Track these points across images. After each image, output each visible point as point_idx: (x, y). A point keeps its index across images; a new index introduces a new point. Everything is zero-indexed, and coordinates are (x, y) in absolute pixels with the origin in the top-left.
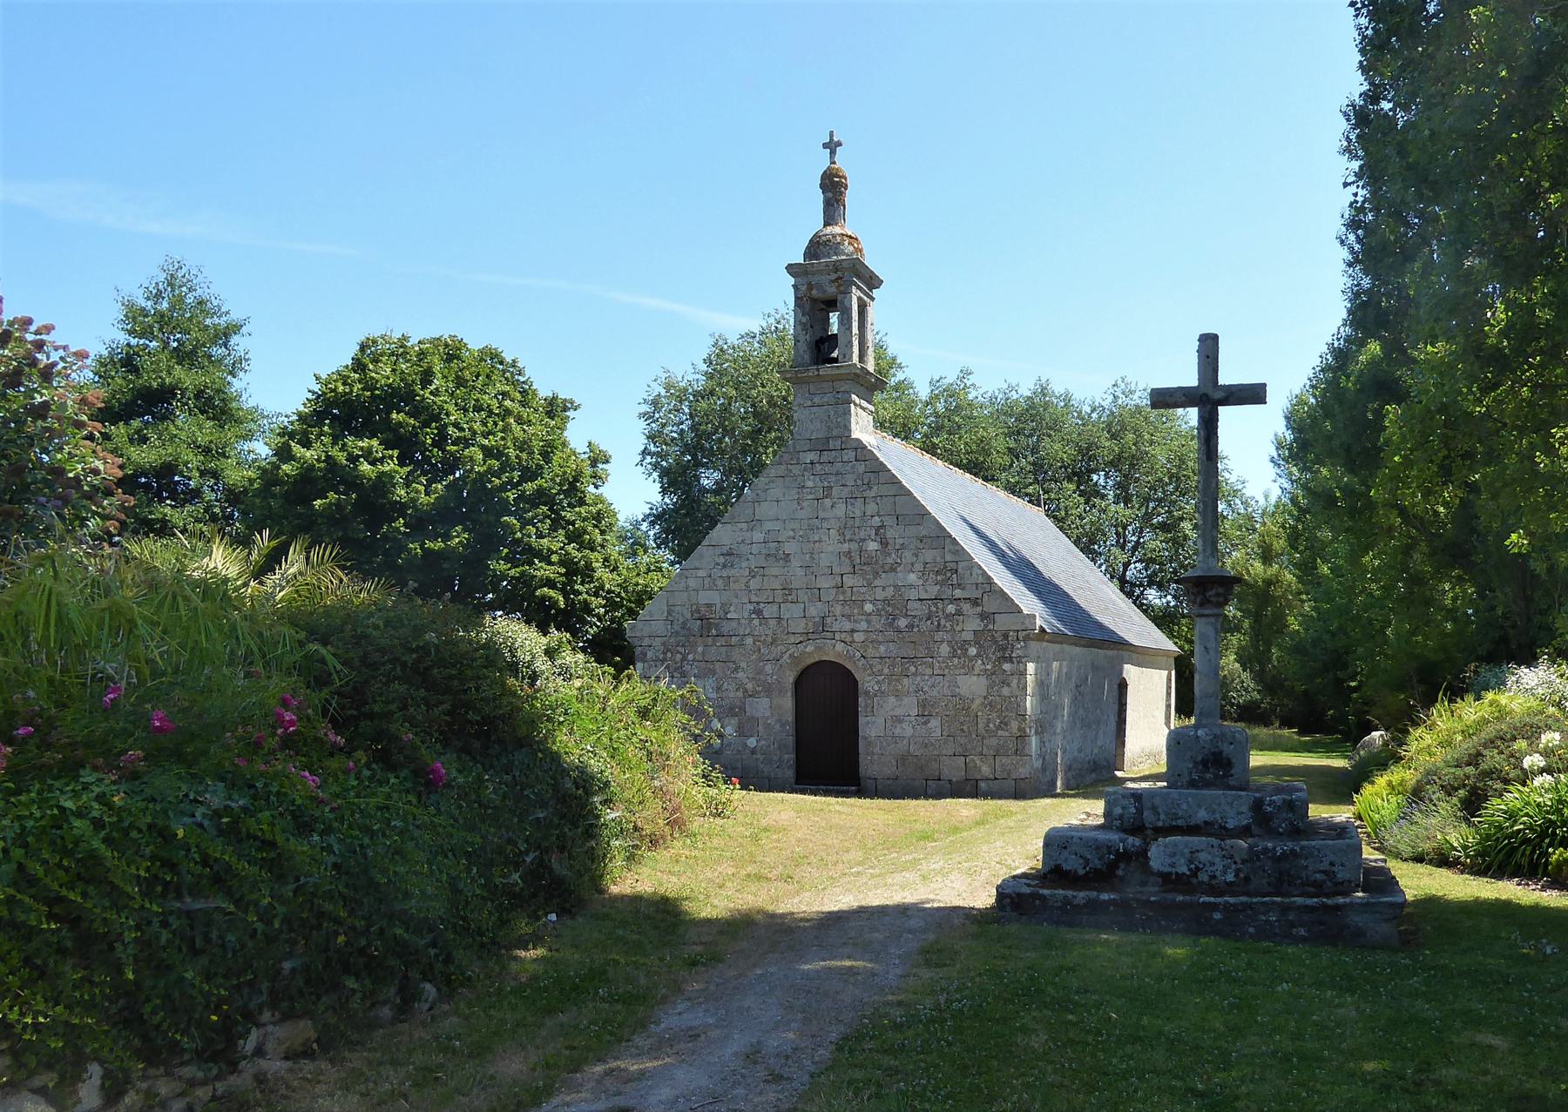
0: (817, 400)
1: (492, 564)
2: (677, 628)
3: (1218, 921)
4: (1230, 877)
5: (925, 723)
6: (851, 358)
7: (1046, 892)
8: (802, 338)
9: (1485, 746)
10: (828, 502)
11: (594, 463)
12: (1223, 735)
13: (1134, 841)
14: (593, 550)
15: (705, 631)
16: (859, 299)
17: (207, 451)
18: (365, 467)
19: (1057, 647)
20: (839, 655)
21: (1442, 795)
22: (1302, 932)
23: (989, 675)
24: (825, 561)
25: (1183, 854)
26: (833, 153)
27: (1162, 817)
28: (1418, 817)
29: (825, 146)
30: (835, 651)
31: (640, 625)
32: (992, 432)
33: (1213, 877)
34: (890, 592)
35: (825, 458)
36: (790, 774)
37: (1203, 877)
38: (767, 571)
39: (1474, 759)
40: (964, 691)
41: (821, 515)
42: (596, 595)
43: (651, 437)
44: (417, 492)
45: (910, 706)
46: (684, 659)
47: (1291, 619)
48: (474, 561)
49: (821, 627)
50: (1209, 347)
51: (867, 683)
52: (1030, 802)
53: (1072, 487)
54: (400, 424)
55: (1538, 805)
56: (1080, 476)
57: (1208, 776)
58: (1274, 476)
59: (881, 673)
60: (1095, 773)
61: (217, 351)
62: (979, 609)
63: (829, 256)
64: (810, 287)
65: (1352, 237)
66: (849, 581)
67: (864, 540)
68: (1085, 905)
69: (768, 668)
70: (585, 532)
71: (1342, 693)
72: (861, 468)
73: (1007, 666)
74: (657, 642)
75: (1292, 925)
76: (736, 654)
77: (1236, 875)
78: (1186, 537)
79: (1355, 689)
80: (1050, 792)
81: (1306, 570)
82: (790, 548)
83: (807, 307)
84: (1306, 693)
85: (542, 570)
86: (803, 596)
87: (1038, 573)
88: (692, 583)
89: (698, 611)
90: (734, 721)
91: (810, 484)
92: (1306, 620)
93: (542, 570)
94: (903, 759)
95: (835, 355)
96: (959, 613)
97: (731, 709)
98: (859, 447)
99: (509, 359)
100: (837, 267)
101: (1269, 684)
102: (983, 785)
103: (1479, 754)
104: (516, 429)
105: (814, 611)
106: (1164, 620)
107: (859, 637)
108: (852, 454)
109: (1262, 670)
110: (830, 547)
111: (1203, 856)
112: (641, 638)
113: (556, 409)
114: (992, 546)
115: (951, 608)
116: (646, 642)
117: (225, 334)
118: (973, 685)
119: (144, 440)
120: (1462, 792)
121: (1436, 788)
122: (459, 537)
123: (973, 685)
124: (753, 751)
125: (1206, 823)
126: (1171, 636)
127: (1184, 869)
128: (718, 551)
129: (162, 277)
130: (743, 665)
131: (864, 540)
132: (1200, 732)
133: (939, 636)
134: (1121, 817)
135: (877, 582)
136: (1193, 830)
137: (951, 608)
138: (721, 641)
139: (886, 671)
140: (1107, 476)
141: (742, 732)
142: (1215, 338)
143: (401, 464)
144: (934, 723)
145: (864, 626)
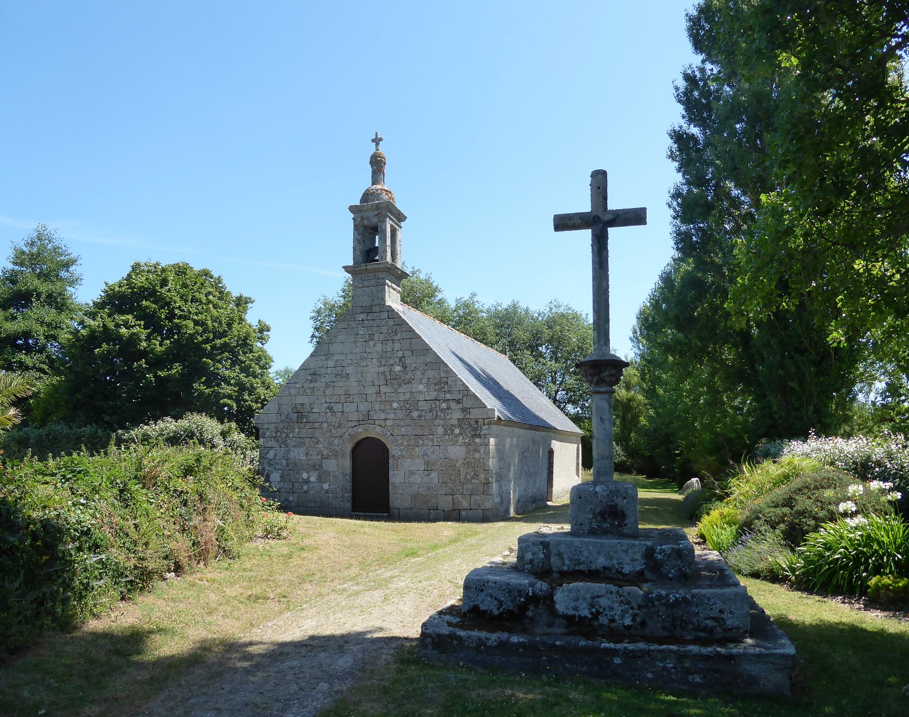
0: (366, 283)
2: (283, 418)
3: (619, 665)
4: (628, 621)
5: (429, 475)
7: (462, 633)
8: (358, 248)
9: (795, 492)
10: (372, 343)
11: (261, 331)
12: (618, 491)
13: (542, 586)
14: (255, 377)
16: (391, 226)
17: (49, 325)
18: (123, 330)
21: (766, 527)
22: (698, 679)
24: (369, 379)
25: (585, 599)
26: (377, 144)
27: (567, 562)
28: (751, 543)
29: (373, 141)
30: (375, 432)
32: (487, 323)
33: (613, 621)
34: (408, 396)
35: (370, 317)
36: (348, 505)
37: (603, 620)
38: (336, 384)
39: (789, 502)
41: (368, 350)
42: (257, 402)
43: (317, 329)
44: (155, 345)
45: (419, 465)
46: (287, 436)
47: (642, 418)
48: (186, 380)
49: (367, 418)
50: (599, 181)
51: (394, 450)
52: (490, 524)
53: (529, 353)
54: (147, 307)
55: (850, 540)
56: (533, 348)
57: (606, 525)
59: (402, 444)
60: (535, 506)
61: (63, 274)
62: (461, 406)
63: (373, 200)
64: (363, 219)
65: (675, 203)
66: (384, 389)
68: (497, 647)
69: (336, 441)
70: (251, 367)
71: (671, 457)
72: (391, 323)
73: (478, 440)
74: (272, 426)
75: (688, 672)
76: (317, 433)
77: (634, 620)
79: (678, 455)
80: (505, 518)
81: (650, 393)
82: (349, 370)
83: (361, 230)
84: (650, 457)
85: (226, 389)
86: (356, 399)
87: (500, 387)
88: (293, 391)
89: (296, 408)
91: (361, 332)
92: (650, 419)
93: (226, 389)
94: (415, 497)
95: (377, 258)
97: (314, 466)
98: (390, 310)
99: (216, 276)
100: (378, 207)
101: (631, 452)
102: (463, 513)
103: (791, 498)
104: (214, 311)
105: (363, 407)
106: (576, 419)
108: (385, 315)
109: (627, 445)
110: (373, 368)
111: (603, 602)
113: (242, 303)
114: (471, 369)
115: (444, 405)
117: (67, 265)
118: (457, 452)
119: (14, 318)
120: (782, 526)
121: (762, 522)
122: (177, 368)
123: (457, 452)
124: (327, 492)
125: (604, 568)
126: (581, 428)
127: (585, 613)
129: (36, 234)
130: (322, 440)
132: (598, 489)
133: (437, 422)
134: (531, 562)
135: (400, 390)
136: (593, 575)
137: (444, 405)
140: (547, 348)
141: (320, 480)
142: (604, 173)
143: (145, 328)
144: (434, 475)
145: (392, 416)
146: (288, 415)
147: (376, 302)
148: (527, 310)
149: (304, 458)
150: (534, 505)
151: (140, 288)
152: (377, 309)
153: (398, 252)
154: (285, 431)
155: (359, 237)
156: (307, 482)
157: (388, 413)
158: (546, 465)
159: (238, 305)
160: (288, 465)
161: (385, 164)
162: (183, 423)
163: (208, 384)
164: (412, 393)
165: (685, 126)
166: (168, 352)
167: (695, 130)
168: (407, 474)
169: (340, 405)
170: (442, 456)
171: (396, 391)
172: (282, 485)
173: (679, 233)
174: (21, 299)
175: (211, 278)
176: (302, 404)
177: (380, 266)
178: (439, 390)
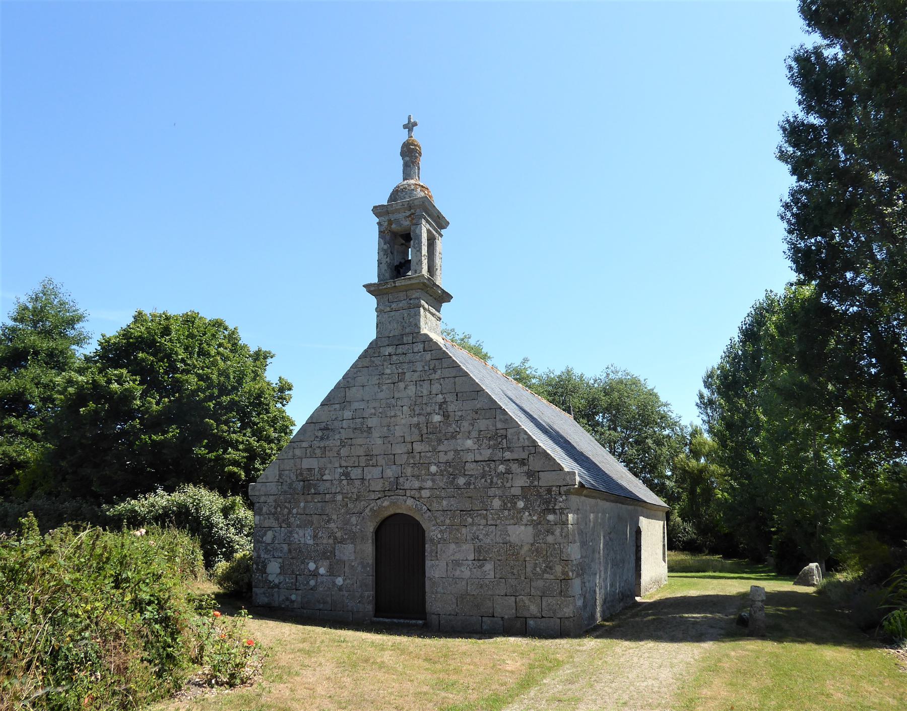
0: (394, 306)
1: (196, 450)
2: (285, 487)
5: (481, 567)
6: (421, 272)
8: (384, 261)
10: (402, 385)
15: (306, 490)
17: (46, 386)
18: (115, 386)
19: (592, 501)
20: (410, 509)
23: (535, 524)
24: (398, 433)
29: (405, 127)
30: (407, 506)
31: (259, 486)
34: (451, 455)
35: (400, 351)
38: (354, 441)
40: (513, 539)
44: (150, 403)
45: (467, 551)
48: (184, 444)
49: (395, 487)
51: (432, 532)
54: (143, 360)
58: (698, 414)
62: (526, 468)
64: (390, 222)
65: (789, 214)
66: (418, 447)
67: (429, 414)
69: (354, 520)
72: (428, 356)
73: (551, 517)
76: (329, 509)
78: (649, 448)
82: (372, 422)
83: (388, 237)
85: (232, 454)
86: (381, 461)
88: (298, 452)
89: (301, 474)
90: (326, 563)
91: (388, 371)
93: (232, 454)
96: (508, 472)
97: (324, 553)
101: (702, 529)
102: (531, 622)
104: (221, 364)
105: (389, 473)
107: (425, 493)
108: (421, 346)
110: (403, 420)
112: (259, 496)
113: (261, 357)
115: (502, 468)
116: (262, 499)
117: (71, 322)
118: (521, 534)
122: (173, 432)
123: (521, 534)
124: (340, 589)
128: (318, 427)
130: (334, 517)
131: (429, 414)
133: (491, 492)
137: (502, 468)
138: (318, 498)
139: (448, 521)
140: (604, 417)
141: (332, 572)
143: (141, 384)
144: (488, 567)
145: (429, 484)
146: (291, 484)
147: (408, 330)
148: (581, 377)
149: (311, 542)
150: (621, 604)
151: (136, 338)
152: (409, 339)
153: (438, 267)
154: (287, 505)
155: (385, 247)
156: (315, 574)
157: (423, 480)
158: (634, 549)
159: (255, 360)
160: (290, 551)
161: (420, 154)
162: (177, 497)
163: (211, 448)
164: (456, 451)
165: (801, 115)
166: (166, 411)
167: (814, 120)
168: (450, 565)
169: (359, 470)
170: (499, 540)
171: (434, 450)
172: (282, 578)
173: (795, 250)
174: (16, 358)
175: (226, 329)
176: (310, 470)
177: (413, 282)
178: (494, 447)
